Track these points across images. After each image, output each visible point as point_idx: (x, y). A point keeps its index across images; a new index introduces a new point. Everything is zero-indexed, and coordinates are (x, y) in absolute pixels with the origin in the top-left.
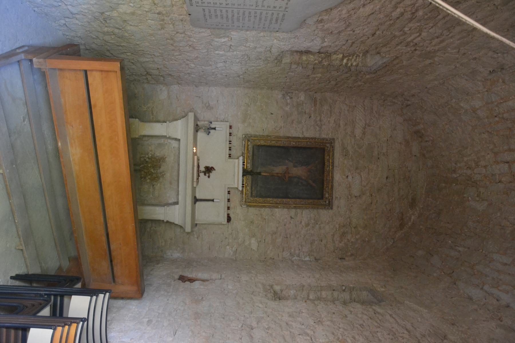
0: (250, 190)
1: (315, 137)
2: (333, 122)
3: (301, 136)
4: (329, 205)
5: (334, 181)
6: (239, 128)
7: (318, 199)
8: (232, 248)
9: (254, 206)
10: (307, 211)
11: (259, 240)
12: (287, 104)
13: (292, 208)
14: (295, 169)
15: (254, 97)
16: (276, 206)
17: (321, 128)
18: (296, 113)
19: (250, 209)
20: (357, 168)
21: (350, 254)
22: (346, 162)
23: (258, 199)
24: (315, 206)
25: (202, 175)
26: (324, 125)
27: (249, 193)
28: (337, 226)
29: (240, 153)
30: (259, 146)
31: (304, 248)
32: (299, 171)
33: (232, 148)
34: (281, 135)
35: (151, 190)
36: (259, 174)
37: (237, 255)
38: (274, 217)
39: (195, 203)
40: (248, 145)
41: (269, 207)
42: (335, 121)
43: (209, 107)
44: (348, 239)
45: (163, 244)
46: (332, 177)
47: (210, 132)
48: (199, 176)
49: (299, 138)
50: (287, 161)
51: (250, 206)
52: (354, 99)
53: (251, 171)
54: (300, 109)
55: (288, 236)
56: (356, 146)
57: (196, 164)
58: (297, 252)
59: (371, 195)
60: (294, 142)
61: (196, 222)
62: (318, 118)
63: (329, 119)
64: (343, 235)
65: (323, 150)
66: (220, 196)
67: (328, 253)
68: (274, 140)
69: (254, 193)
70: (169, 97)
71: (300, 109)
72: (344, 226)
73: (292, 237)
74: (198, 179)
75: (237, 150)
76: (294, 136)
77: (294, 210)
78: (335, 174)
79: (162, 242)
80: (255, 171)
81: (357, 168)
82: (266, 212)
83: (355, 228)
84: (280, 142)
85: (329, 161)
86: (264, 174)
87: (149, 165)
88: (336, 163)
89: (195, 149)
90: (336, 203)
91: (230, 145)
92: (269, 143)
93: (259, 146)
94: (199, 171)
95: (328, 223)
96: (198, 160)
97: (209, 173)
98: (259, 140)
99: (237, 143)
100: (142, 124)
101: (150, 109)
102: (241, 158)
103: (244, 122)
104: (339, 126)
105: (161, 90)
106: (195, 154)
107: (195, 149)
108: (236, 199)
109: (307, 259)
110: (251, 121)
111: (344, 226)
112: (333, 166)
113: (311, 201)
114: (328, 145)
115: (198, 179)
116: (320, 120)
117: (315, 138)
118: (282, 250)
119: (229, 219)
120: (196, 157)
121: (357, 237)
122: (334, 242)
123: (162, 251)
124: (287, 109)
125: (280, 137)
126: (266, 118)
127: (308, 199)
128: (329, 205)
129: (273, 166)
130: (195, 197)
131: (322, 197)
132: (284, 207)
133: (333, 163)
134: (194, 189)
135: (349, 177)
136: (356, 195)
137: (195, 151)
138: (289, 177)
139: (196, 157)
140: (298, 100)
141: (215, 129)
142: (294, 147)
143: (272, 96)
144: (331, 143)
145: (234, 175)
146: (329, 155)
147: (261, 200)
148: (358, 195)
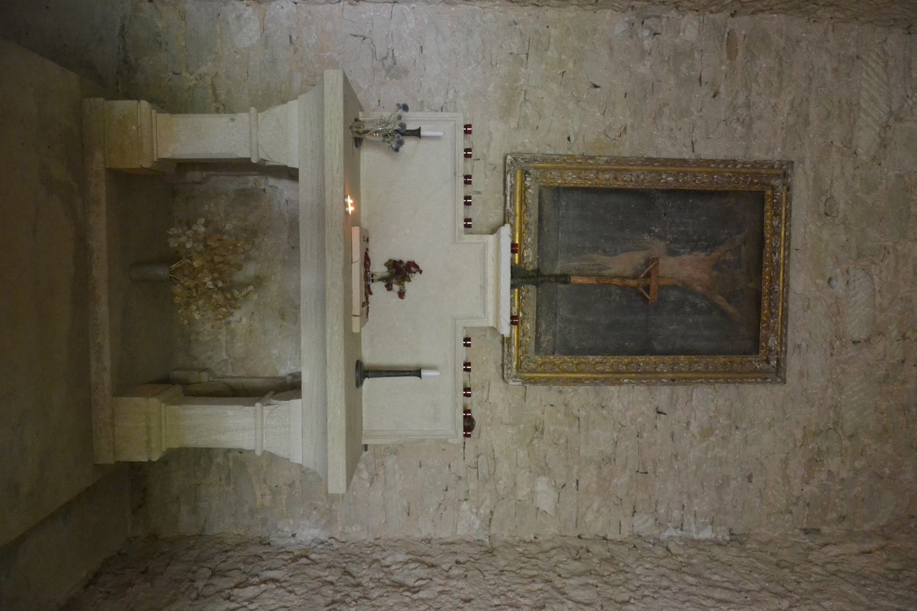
0: (531, 333)
1: (730, 156)
2: (787, 108)
3: (686, 157)
4: (778, 374)
5: (791, 296)
6: (490, 134)
7: (745, 353)
8: (478, 508)
9: (547, 382)
10: (707, 389)
11: (560, 481)
12: (644, 54)
13: (664, 384)
14: (671, 260)
15: (537, 32)
16: (615, 378)
17: (749, 127)
18: (672, 82)
19: (531, 388)
20: (860, 255)
21: (835, 515)
22: (825, 235)
23: (557, 359)
24: (734, 376)
25: (378, 288)
26: (760, 118)
27: (530, 341)
28: (799, 434)
29: (496, 216)
30: (558, 190)
31: (696, 501)
32: (684, 267)
33: (475, 199)
34: (626, 154)
35: (223, 337)
36: (564, 278)
37: (493, 530)
38: (605, 412)
39: (359, 384)
40: (524, 189)
41: (594, 382)
42: (792, 106)
43: (393, 69)
44: (830, 473)
45: (267, 500)
46: (786, 284)
47: (401, 143)
48: (368, 291)
49: (685, 161)
50: (646, 237)
51: (535, 382)
52: (854, 33)
53: (538, 271)
54: (683, 69)
55: (650, 468)
56: (858, 185)
57: (357, 256)
58: (676, 513)
59: (904, 337)
60: (670, 175)
61: (364, 442)
62: (741, 100)
63: (773, 101)
64: (815, 461)
65: (760, 198)
66: (438, 351)
67: (769, 515)
68: (604, 171)
69: (546, 340)
70: (266, 40)
71: (683, 69)
72: (817, 434)
73: (661, 470)
74: (365, 304)
75: (488, 208)
76: (664, 155)
77: (667, 390)
78: (792, 273)
79: (263, 496)
80: (546, 272)
81: (860, 255)
82: (580, 397)
83: (851, 437)
84: (627, 177)
85: (776, 232)
86: (580, 280)
87: (196, 264)
88: (797, 240)
89: (350, 201)
90: (793, 363)
91: (470, 189)
92: (590, 179)
93: (558, 189)
94: (368, 278)
95: (770, 425)
96: (366, 240)
97: (400, 283)
98: (562, 170)
99: (487, 184)
100: (163, 118)
101: (208, 79)
102: (506, 230)
103: (506, 112)
104: (807, 123)
105: (239, 17)
106: (353, 220)
107: (350, 201)
108: (487, 360)
109: (707, 534)
110: (528, 110)
111: (817, 434)
112: (788, 248)
113: (722, 359)
114: (777, 182)
115: (365, 304)
116: (748, 105)
117: (735, 162)
118: (629, 511)
119: (469, 425)
120: (356, 231)
121: (857, 464)
122: (787, 480)
123: (264, 522)
124: (643, 69)
125: (626, 161)
126: (578, 101)
127: (711, 353)
128: (778, 374)
129: (605, 252)
130: (359, 364)
131: (755, 346)
132: (639, 382)
133: (788, 239)
134: (352, 341)
135: (834, 282)
136: (856, 337)
137: (351, 209)
138: (661, 288)
139: (356, 231)
140: (677, 41)
141: (417, 133)
142: (670, 192)
143: (595, 30)
144: (785, 175)
145: (483, 288)
146: (777, 214)
147: (569, 361)
148: (863, 337)
